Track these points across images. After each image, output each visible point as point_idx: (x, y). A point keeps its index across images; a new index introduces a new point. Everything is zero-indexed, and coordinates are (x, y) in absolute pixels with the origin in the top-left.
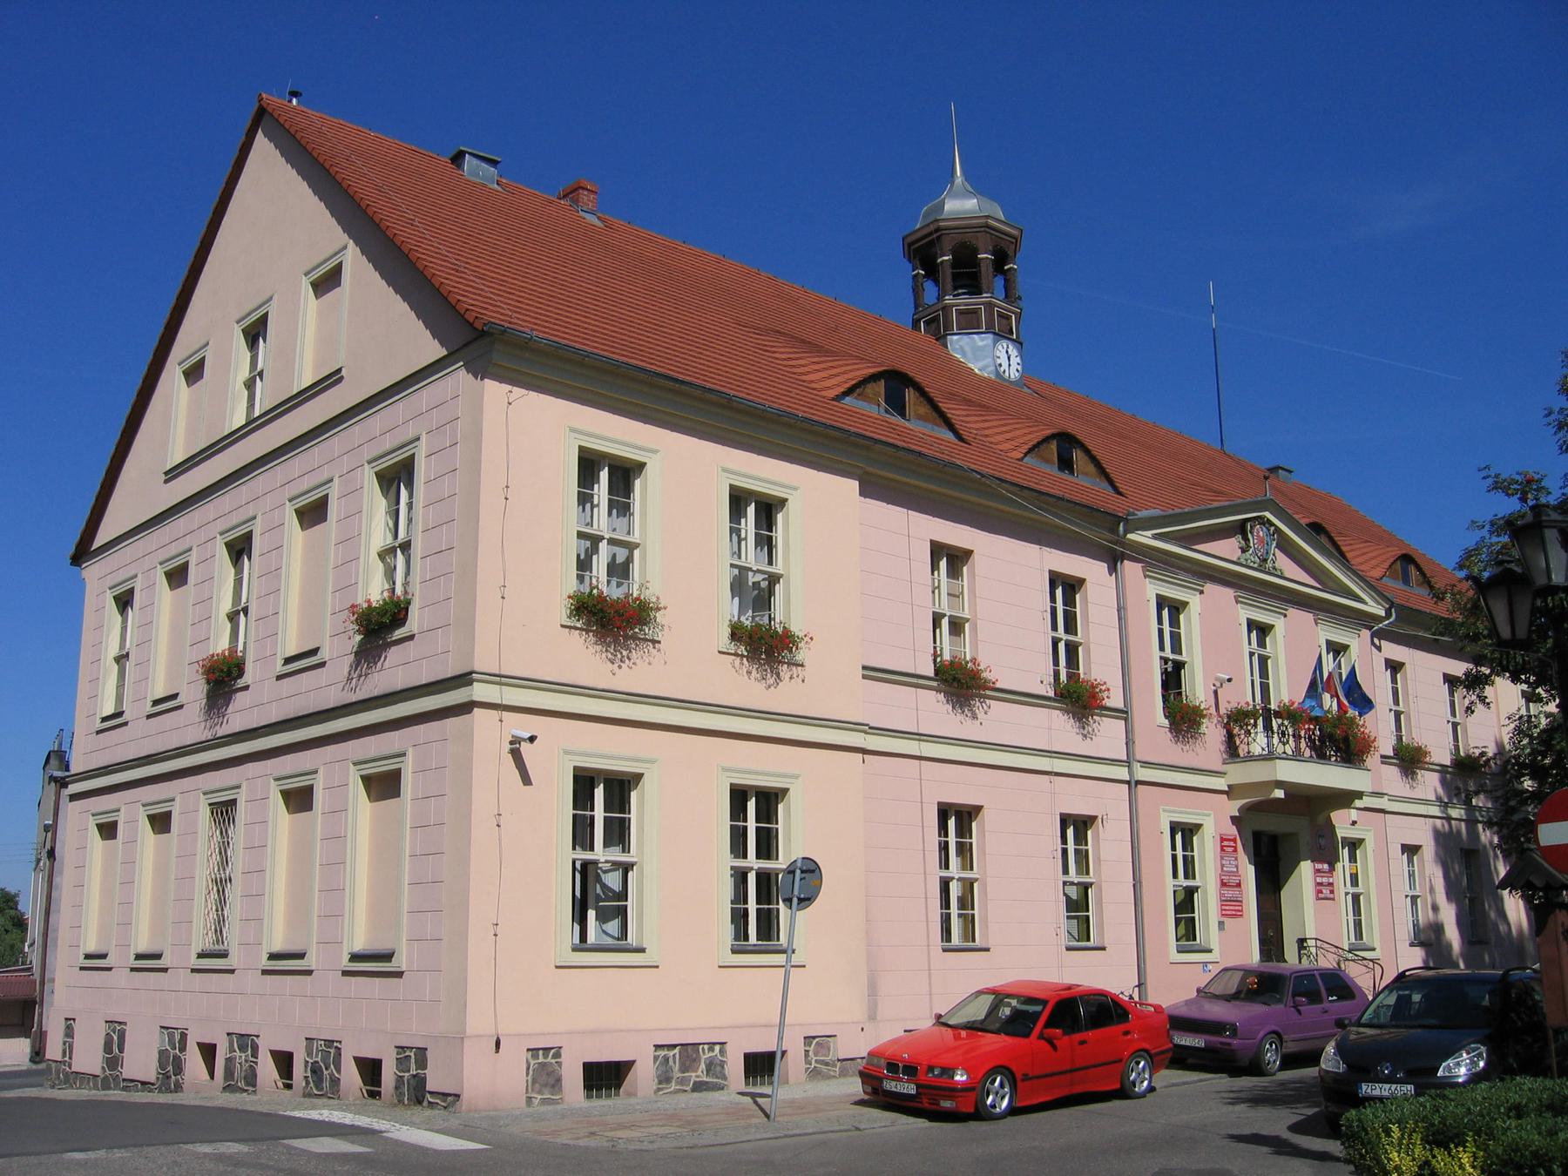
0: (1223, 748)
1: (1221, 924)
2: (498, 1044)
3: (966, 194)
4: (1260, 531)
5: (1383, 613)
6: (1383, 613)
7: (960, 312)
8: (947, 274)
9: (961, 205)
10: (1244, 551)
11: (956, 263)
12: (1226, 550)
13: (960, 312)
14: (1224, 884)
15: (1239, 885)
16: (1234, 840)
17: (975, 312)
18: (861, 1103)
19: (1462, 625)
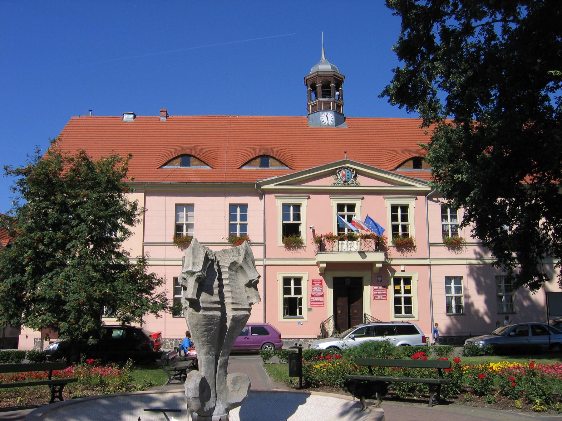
0: (180, 250)
1: (310, 310)
2: (27, 337)
3: (325, 64)
4: (343, 172)
5: (429, 189)
6: (429, 189)
7: (324, 104)
8: (319, 91)
9: (324, 67)
10: (336, 179)
11: (323, 87)
12: (327, 182)
13: (324, 104)
14: (312, 296)
15: (323, 296)
16: (321, 281)
17: (329, 104)
18: (357, 419)
19: (550, 179)
